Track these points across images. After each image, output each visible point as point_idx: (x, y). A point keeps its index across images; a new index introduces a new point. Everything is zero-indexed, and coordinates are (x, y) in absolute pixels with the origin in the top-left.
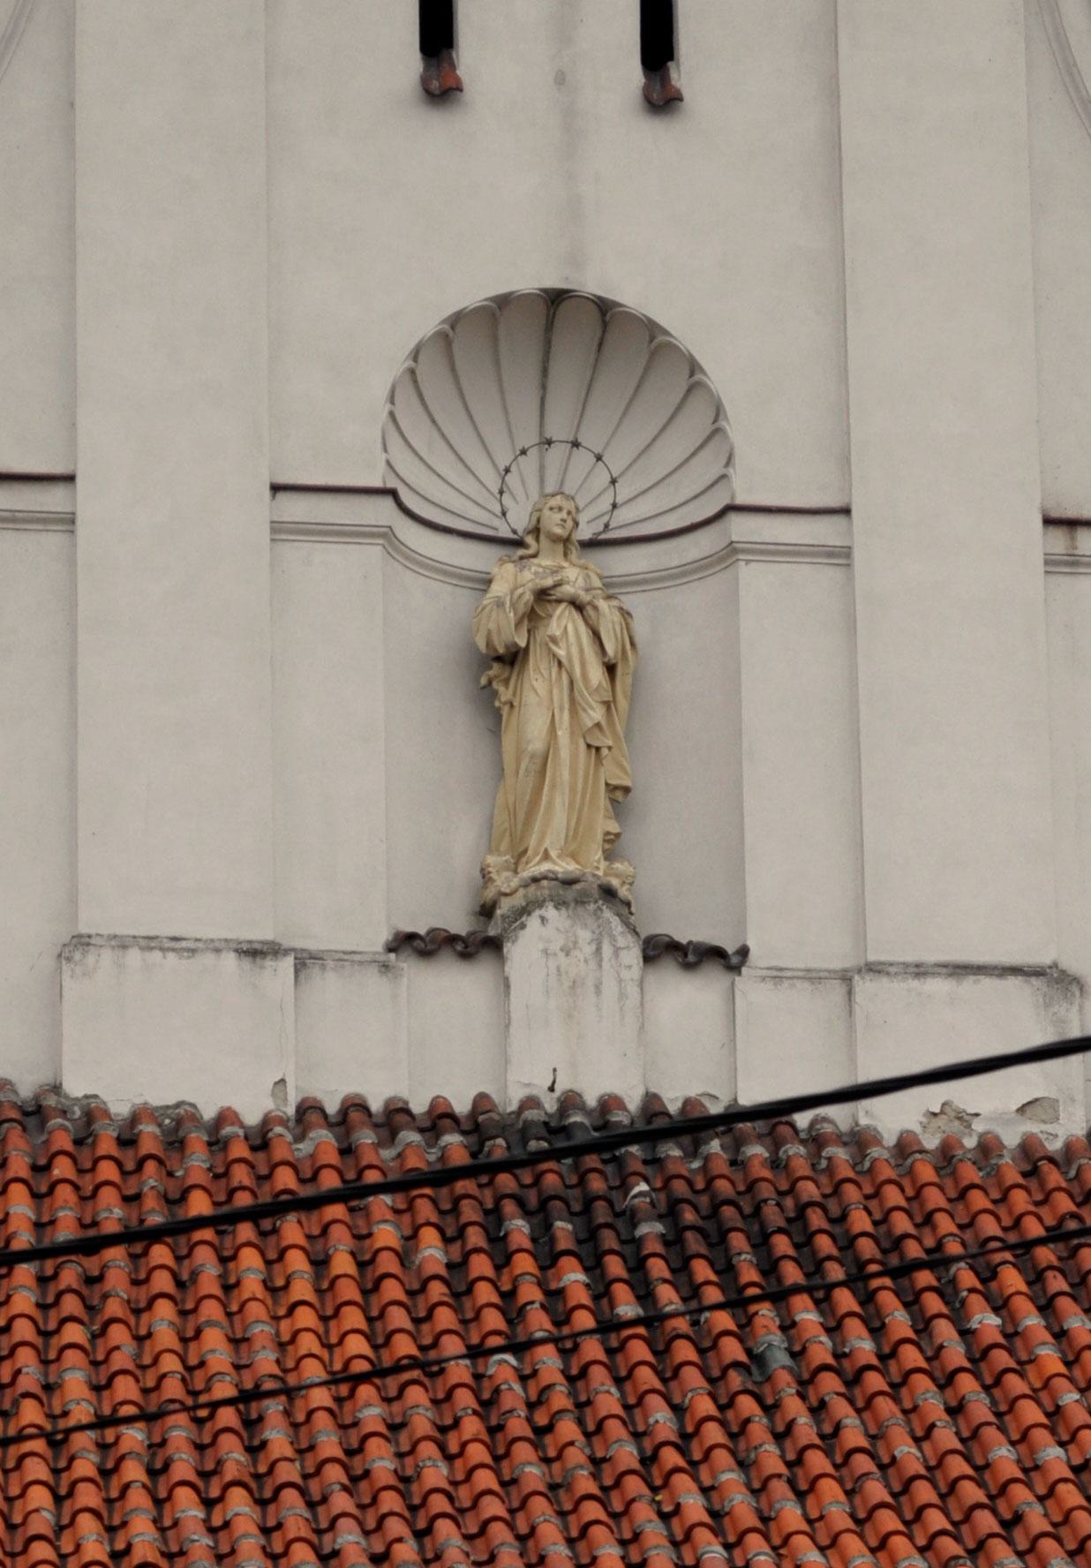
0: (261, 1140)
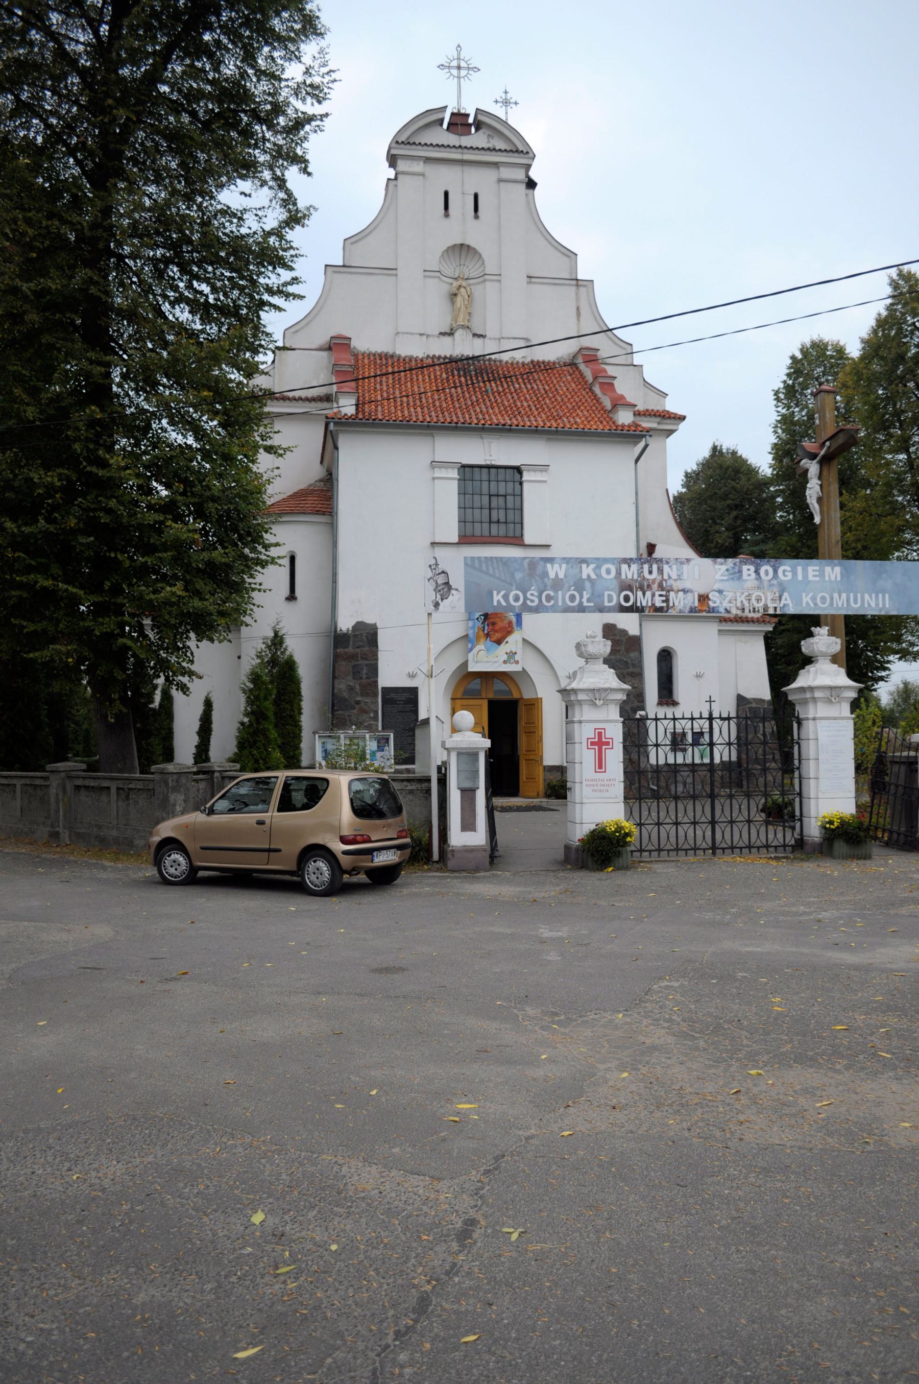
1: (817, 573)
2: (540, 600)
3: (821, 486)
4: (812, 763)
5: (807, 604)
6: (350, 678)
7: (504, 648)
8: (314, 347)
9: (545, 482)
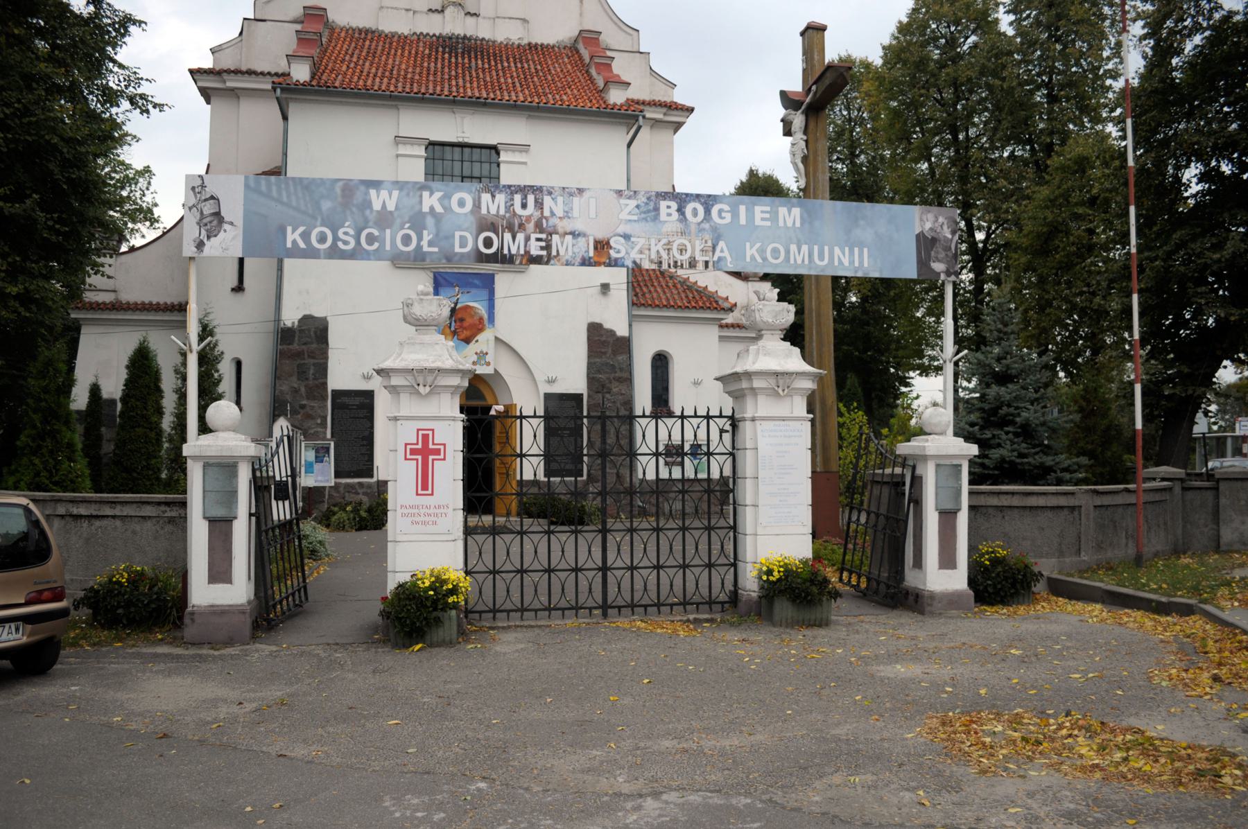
0: (406, 37)
1: (767, 216)
2: (358, 242)
3: (806, 141)
4: (749, 484)
5: (753, 258)
6: (294, 378)
7: (473, 347)
8: (288, 19)
9: (525, 163)
